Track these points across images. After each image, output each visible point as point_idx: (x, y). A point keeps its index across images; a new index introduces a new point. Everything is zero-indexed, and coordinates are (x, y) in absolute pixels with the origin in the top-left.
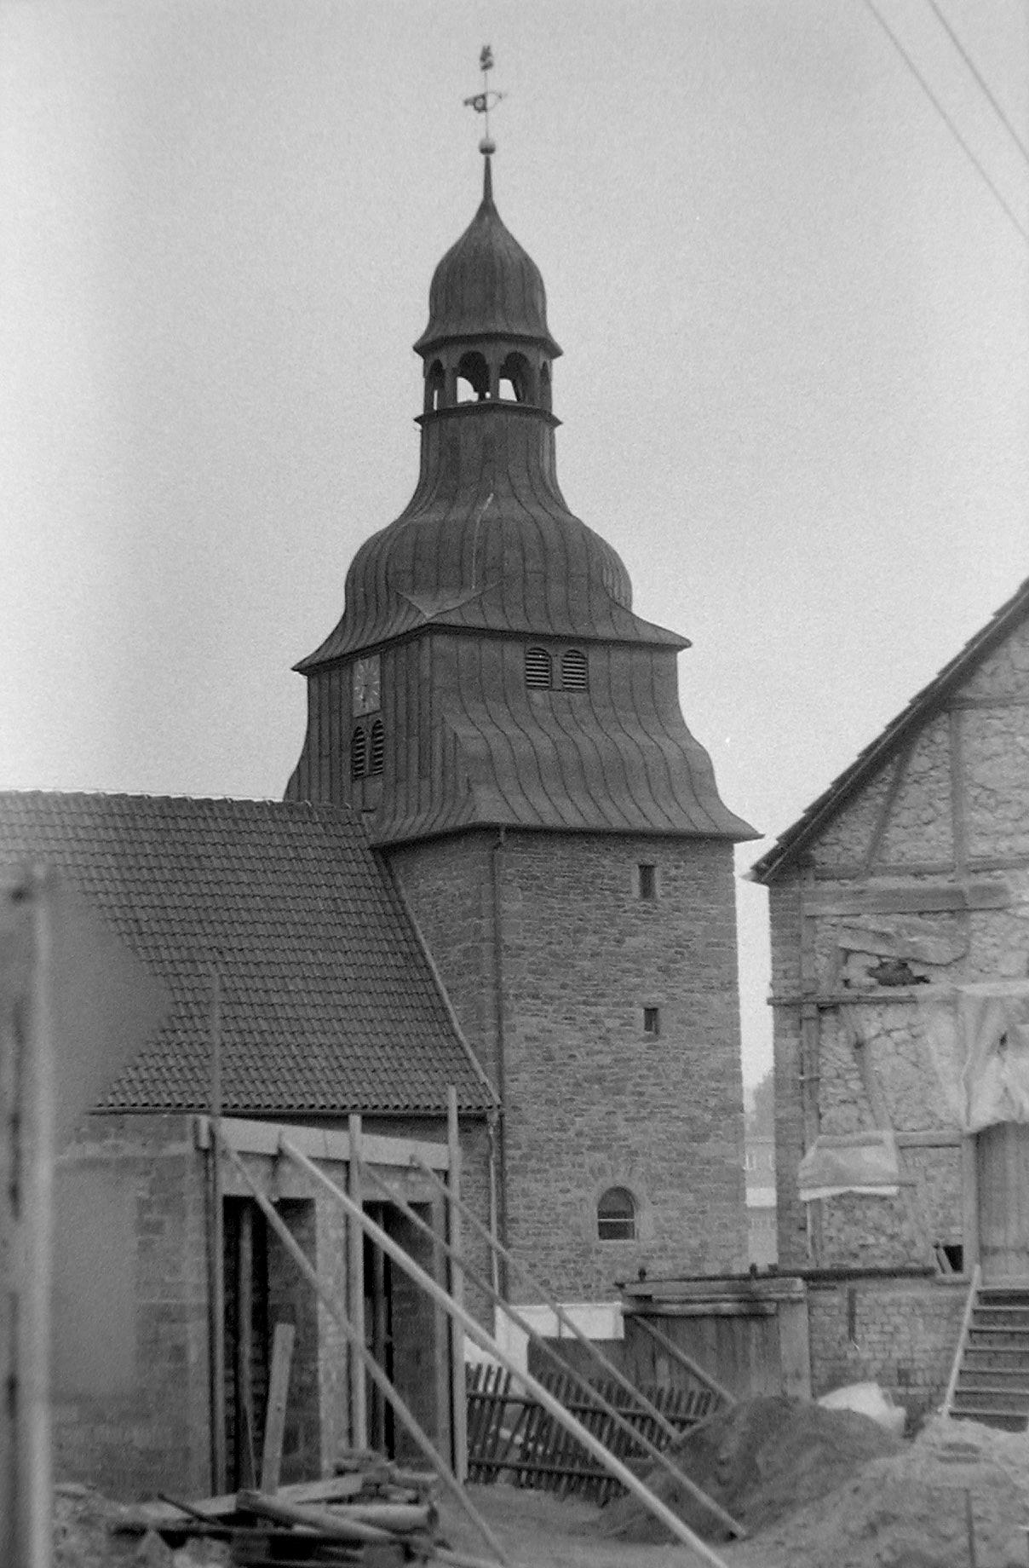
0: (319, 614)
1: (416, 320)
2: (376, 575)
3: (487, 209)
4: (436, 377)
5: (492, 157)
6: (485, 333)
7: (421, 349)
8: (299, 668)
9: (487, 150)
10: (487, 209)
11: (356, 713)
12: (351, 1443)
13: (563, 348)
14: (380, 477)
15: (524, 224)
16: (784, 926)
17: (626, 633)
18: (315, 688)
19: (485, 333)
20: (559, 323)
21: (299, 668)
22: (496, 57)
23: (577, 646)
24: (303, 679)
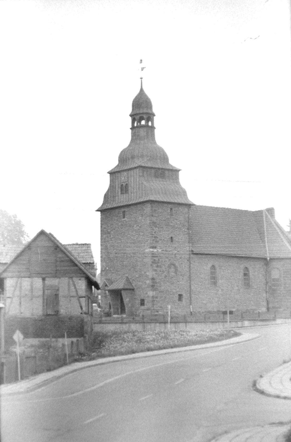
0: (114, 163)
1: (130, 110)
2: (124, 158)
3: (142, 90)
4: (133, 121)
5: (142, 80)
6: (142, 113)
7: (131, 116)
8: (108, 173)
9: (141, 78)
10: (142, 90)
11: (122, 181)
12: (82, 308)
13: (156, 114)
14: (124, 139)
15: (148, 92)
16: (261, 226)
17: (168, 168)
18: (112, 177)
19: (142, 113)
20: (155, 110)
21: (108, 173)
22: (139, 61)
23: (163, 170)
24: (109, 175)
